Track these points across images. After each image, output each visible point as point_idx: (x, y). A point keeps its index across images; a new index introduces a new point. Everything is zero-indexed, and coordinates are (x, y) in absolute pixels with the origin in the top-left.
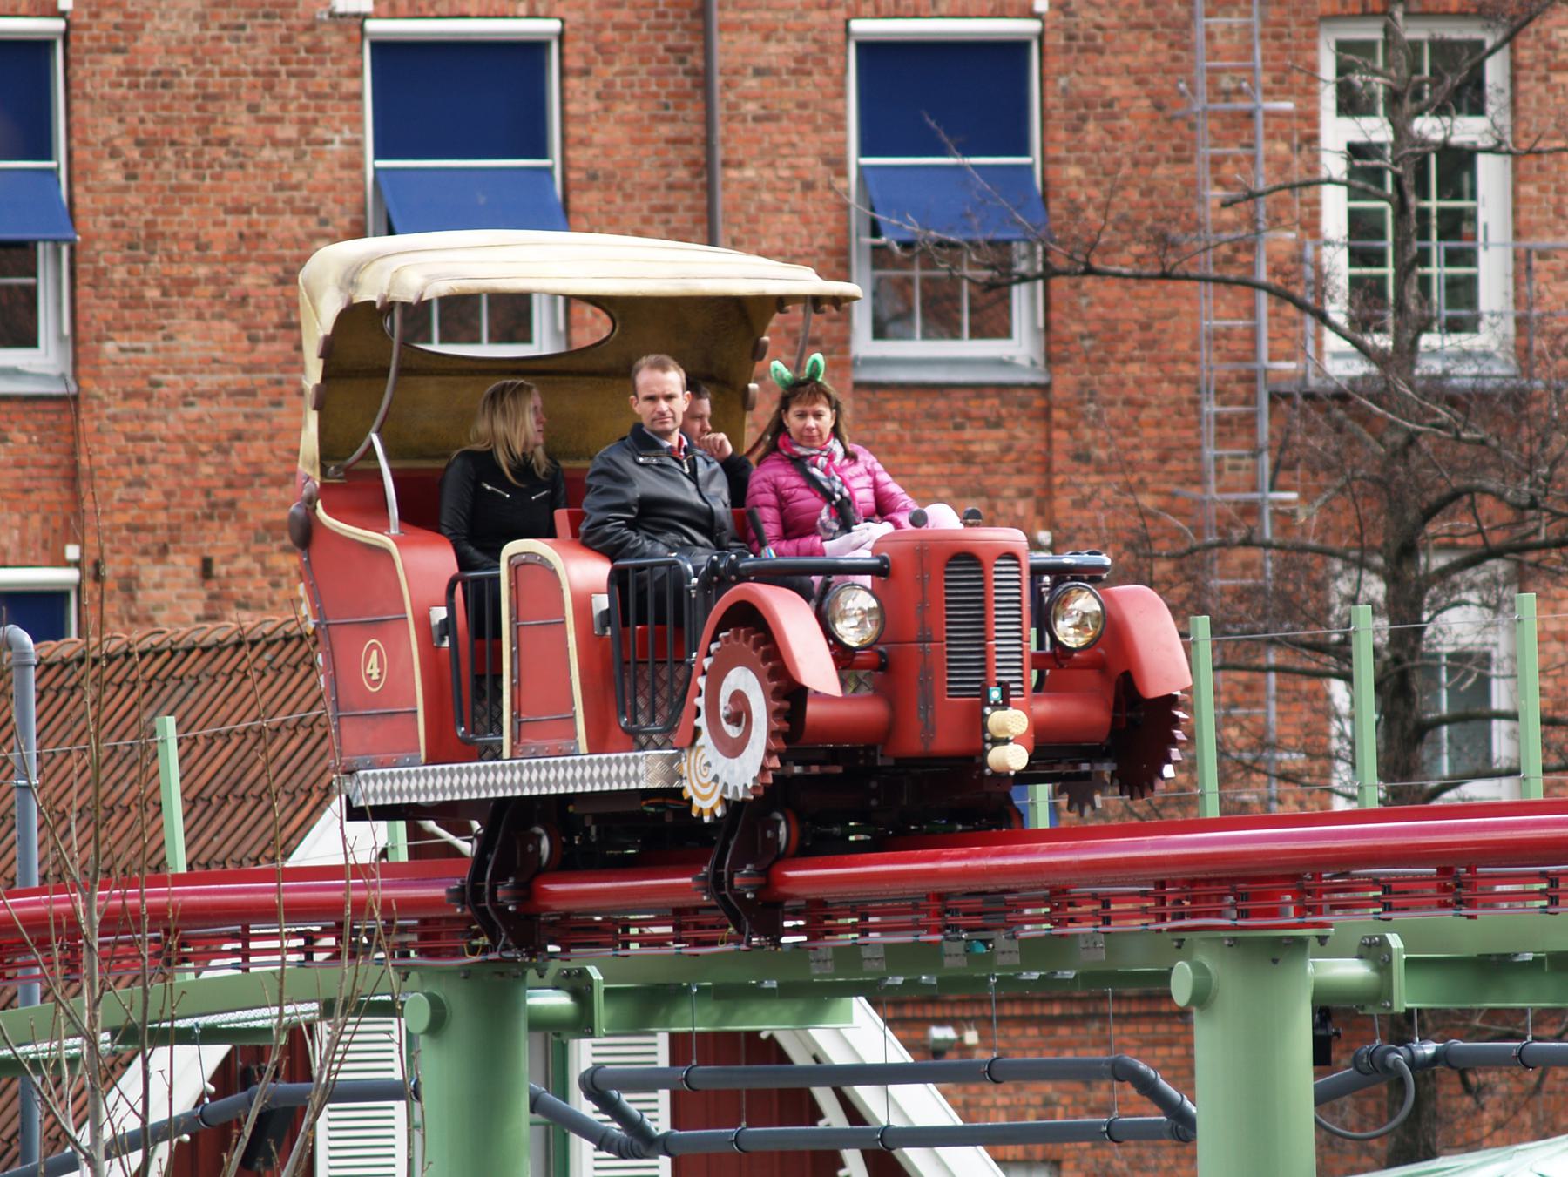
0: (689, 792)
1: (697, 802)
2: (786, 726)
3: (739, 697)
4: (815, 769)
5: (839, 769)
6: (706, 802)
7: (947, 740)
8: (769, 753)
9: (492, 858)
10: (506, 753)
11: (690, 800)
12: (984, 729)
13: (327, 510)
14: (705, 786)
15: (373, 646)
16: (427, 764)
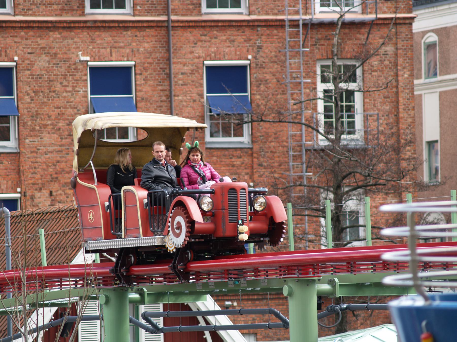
0: (167, 246)
1: (169, 248)
2: (190, 230)
3: (179, 223)
4: (197, 240)
5: (203, 240)
6: (171, 248)
7: (228, 233)
8: (186, 236)
9: (120, 262)
10: (123, 237)
11: (167, 248)
12: (238, 230)
13: (80, 179)
14: (171, 244)
15: (91, 212)
16: (104, 239)
